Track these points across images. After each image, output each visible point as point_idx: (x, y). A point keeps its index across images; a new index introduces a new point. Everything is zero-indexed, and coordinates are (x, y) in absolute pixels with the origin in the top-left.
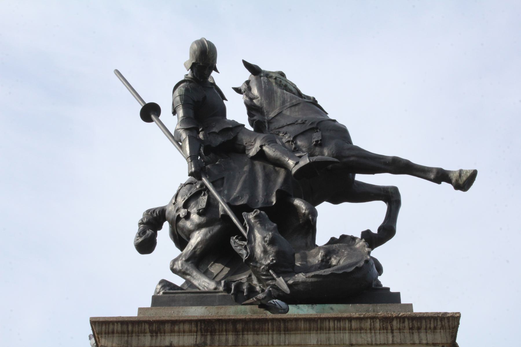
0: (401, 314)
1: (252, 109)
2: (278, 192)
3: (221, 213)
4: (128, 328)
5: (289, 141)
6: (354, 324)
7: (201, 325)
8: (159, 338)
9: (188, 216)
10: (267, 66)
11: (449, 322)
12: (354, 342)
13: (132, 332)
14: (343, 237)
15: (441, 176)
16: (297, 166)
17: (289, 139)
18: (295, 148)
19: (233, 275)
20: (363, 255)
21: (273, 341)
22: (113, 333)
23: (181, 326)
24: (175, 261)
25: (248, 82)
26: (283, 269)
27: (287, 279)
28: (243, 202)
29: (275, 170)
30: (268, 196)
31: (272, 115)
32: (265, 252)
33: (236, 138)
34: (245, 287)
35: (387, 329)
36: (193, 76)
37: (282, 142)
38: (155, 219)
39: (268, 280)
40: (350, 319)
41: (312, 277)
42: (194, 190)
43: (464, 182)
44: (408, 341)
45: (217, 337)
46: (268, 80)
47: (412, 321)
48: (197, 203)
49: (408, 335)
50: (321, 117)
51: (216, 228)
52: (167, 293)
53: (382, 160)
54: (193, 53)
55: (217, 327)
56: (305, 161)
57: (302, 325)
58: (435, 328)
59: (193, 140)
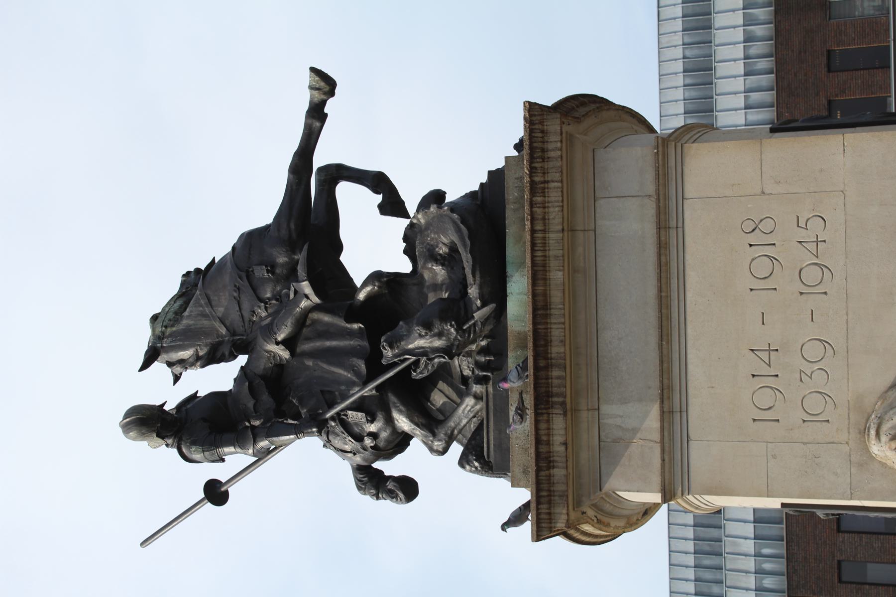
0: (526, 171)
1: (213, 357)
2: (348, 321)
3: (374, 392)
4: (544, 496)
5: (266, 308)
6: (539, 227)
7: (541, 409)
8: (556, 458)
9: (374, 436)
10: (143, 337)
11: (535, 115)
12: (560, 227)
13: (549, 491)
14: (406, 239)
15: (317, 114)
16: (310, 297)
17: (263, 308)
18: (277, 300)
19: (452, 377)
20: (441, 216)
21: (559, 323)
22: (550, 514)
23: (542, 432)
24: (432, 450)
25: (170, 364)
26: (463, 312)
27: (474, 308)
28: (362, 366)
29: (310, 325)
30: (351, 334)
31: (223, 331)
32: (440, 335)
33: (263, 377)
34: (482, 359)
35: (544, 188)
36: (171, 436)
37: (267, 317)
38: (371, 479)
39: (475, 331)
40: (533, 231)
41: (474, 276)
43: (325, 84)
44: (559, 164)
45: (555, 390)
46: (168, 337)
47: (534, 158)
48: (356, 424)
49: (551, 164)
50: (229, 264)
51: (392, 398)
53: (294, 187)
54: (142, 436)
55: (543, 390)
56: (306, 287)
57: (540, 289)
58: (542, 132)
59: (256, 434)
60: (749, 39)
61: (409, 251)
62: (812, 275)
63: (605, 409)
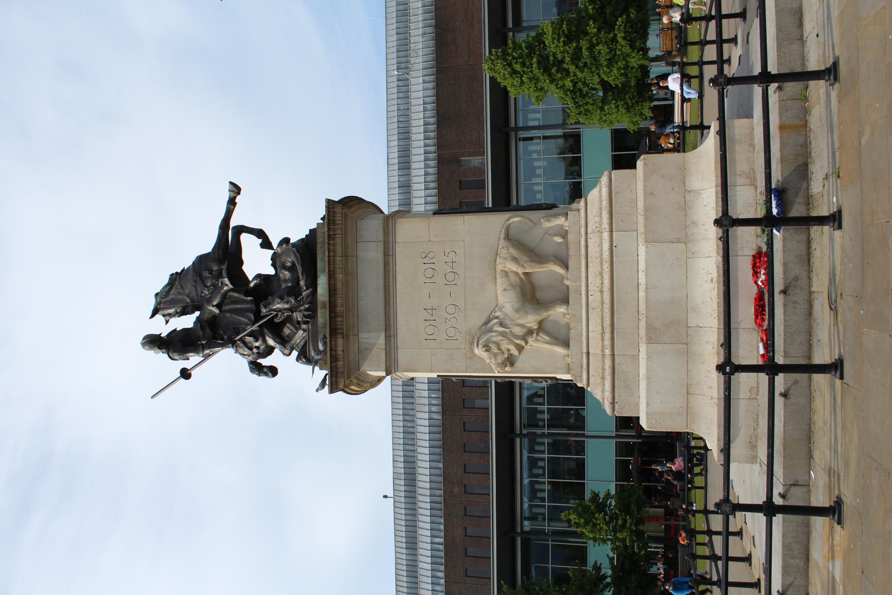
1: (184, 312)
9: (258, 348)
10: (151, 304)
14: (272, 259)
15: (232, 202)
24: (284, 354)
25: (164, 316)
30: (247, 302)
31: (188, 300)
32: (287, 303)
33: (207, 321)
40: (329, 256)
42: (242, 345)
43: (236, 189)
51: (266, 331)
52: (304, 356)
56: (226, 281)
57: (332, 282)
59: (204, 348)
60: (426, 174)
61: (274, 265)
62: (450, 276)
63: (361, 335)
